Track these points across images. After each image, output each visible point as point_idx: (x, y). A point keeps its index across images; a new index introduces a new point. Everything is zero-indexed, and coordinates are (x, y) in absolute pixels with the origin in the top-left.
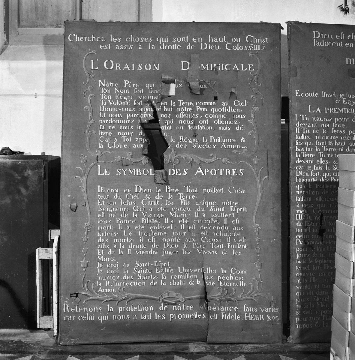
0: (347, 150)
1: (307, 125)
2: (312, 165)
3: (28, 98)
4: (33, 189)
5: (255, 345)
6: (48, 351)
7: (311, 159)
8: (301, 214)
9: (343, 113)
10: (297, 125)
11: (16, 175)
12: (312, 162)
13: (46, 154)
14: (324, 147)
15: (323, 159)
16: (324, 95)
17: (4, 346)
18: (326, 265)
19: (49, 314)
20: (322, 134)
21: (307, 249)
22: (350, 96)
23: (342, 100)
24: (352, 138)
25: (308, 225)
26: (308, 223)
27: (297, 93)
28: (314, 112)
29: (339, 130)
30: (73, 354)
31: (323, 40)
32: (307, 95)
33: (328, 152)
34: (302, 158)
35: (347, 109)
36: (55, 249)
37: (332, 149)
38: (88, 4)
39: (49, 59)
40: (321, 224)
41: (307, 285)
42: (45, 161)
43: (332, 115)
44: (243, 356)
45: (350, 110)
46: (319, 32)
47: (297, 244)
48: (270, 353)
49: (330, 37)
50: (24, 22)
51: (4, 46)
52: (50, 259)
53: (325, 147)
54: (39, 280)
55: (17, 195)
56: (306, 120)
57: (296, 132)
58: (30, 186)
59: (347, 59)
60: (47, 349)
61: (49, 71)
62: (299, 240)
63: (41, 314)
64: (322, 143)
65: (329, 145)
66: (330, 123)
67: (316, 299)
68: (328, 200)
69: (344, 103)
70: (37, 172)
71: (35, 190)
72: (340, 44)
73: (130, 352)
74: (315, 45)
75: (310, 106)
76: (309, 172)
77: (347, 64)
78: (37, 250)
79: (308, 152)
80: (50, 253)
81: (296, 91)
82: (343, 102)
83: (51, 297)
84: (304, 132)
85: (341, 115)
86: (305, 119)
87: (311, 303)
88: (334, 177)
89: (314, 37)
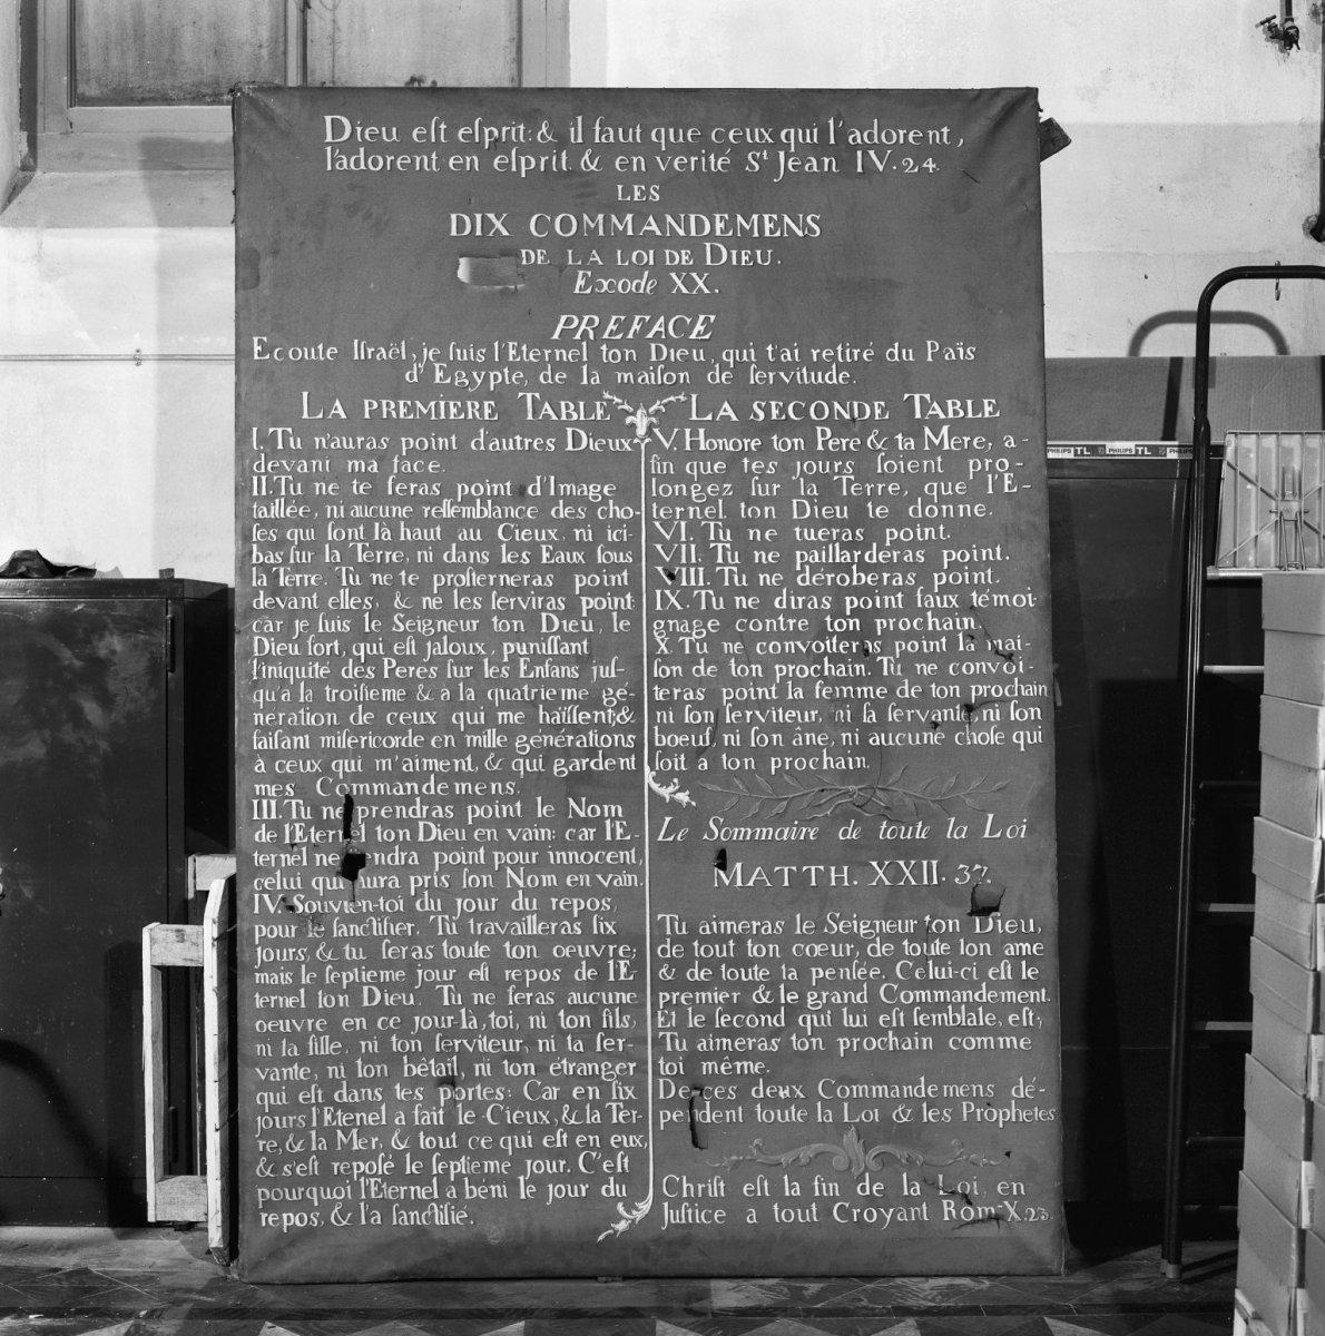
0: (449, 557)
1: (296, 465)
2: (309, 614)
3: (108, 366)
4: (130, 707)
5: (958, 1281)
6: (187, 1307)
7: (308, 591)
8: (272, 798)
9: (433, 418)
10: (259, 466)
11: (66, 655)
12: (311, 602)
13: (177, 576)
14: (355, 547)
15: (353, 591)
16: (359, 350)
17: (25, 1289)
18: (370, 991)
19: (190, 1171)
20: (349, 501)
21: (293, 929)
22: (463, 355)
23: (430, 369)
24: (466, 512)
25: (297, 840)
26: (299, 833)
27: (257, 348)
28: (321, 416)
29: (419, 483)
30: (281, 1317)
31: (362, 150)
32: (295, 354)
33: (372, 567)
34: (274, 590)
35: (452, 404)
36: (210, 929)
37: (388, 554)
38: (328, 16)
39: (163, 221)
40: (347, 835)
41: (296, 1067)
42: (174, 599)
43: (395, 428)
44: (911, 1321)
45: (464, 404)
46: (345, 121)
47: (256, 911)
48: (1008, 1310)
49: (391, 135)
50: (93, 84)
51: (21, 174)
52: (194, 965)
53: (360, 546)
54: (154, 1043)
55: (68, 727)
56: (292, 446)
57: (255, 493)
58: (116, 695)
59: (454, 217)
60: (185, 1301)
61: (167, 270)
62: (266, 896)
63: (161, 1170)
64: (350, 531)
65: (377, 538)
66: (383, 458)
67: (334, 1117)
68: (372, 743)
69: (437, 381)
70: (145, 642)
71: (133, 705)
72: (427, 162)
73: (491, 1310)
74: (329, 168)
75: (305, 394)
76: (301, 641)
77: (454, 233)
78: (146, 931)
79: (298, 568)
80: (193, 944)
81: (256, 339)
82: (434, 376)
83: (199, 1108)
84: (283, 493)
85: (424, 426)
86: (285, 442)
87: (313, 1133)
88: (395, 657)
89: (329, 139)
